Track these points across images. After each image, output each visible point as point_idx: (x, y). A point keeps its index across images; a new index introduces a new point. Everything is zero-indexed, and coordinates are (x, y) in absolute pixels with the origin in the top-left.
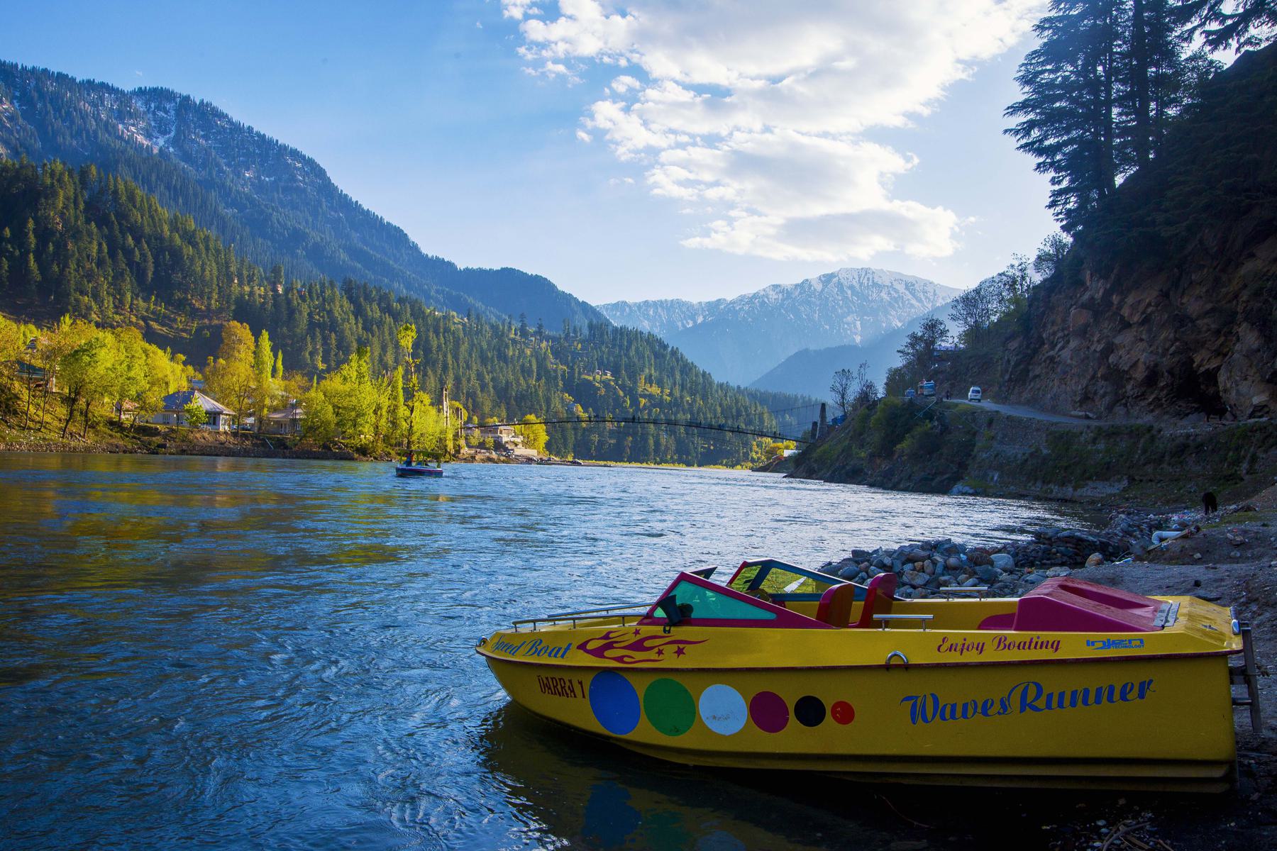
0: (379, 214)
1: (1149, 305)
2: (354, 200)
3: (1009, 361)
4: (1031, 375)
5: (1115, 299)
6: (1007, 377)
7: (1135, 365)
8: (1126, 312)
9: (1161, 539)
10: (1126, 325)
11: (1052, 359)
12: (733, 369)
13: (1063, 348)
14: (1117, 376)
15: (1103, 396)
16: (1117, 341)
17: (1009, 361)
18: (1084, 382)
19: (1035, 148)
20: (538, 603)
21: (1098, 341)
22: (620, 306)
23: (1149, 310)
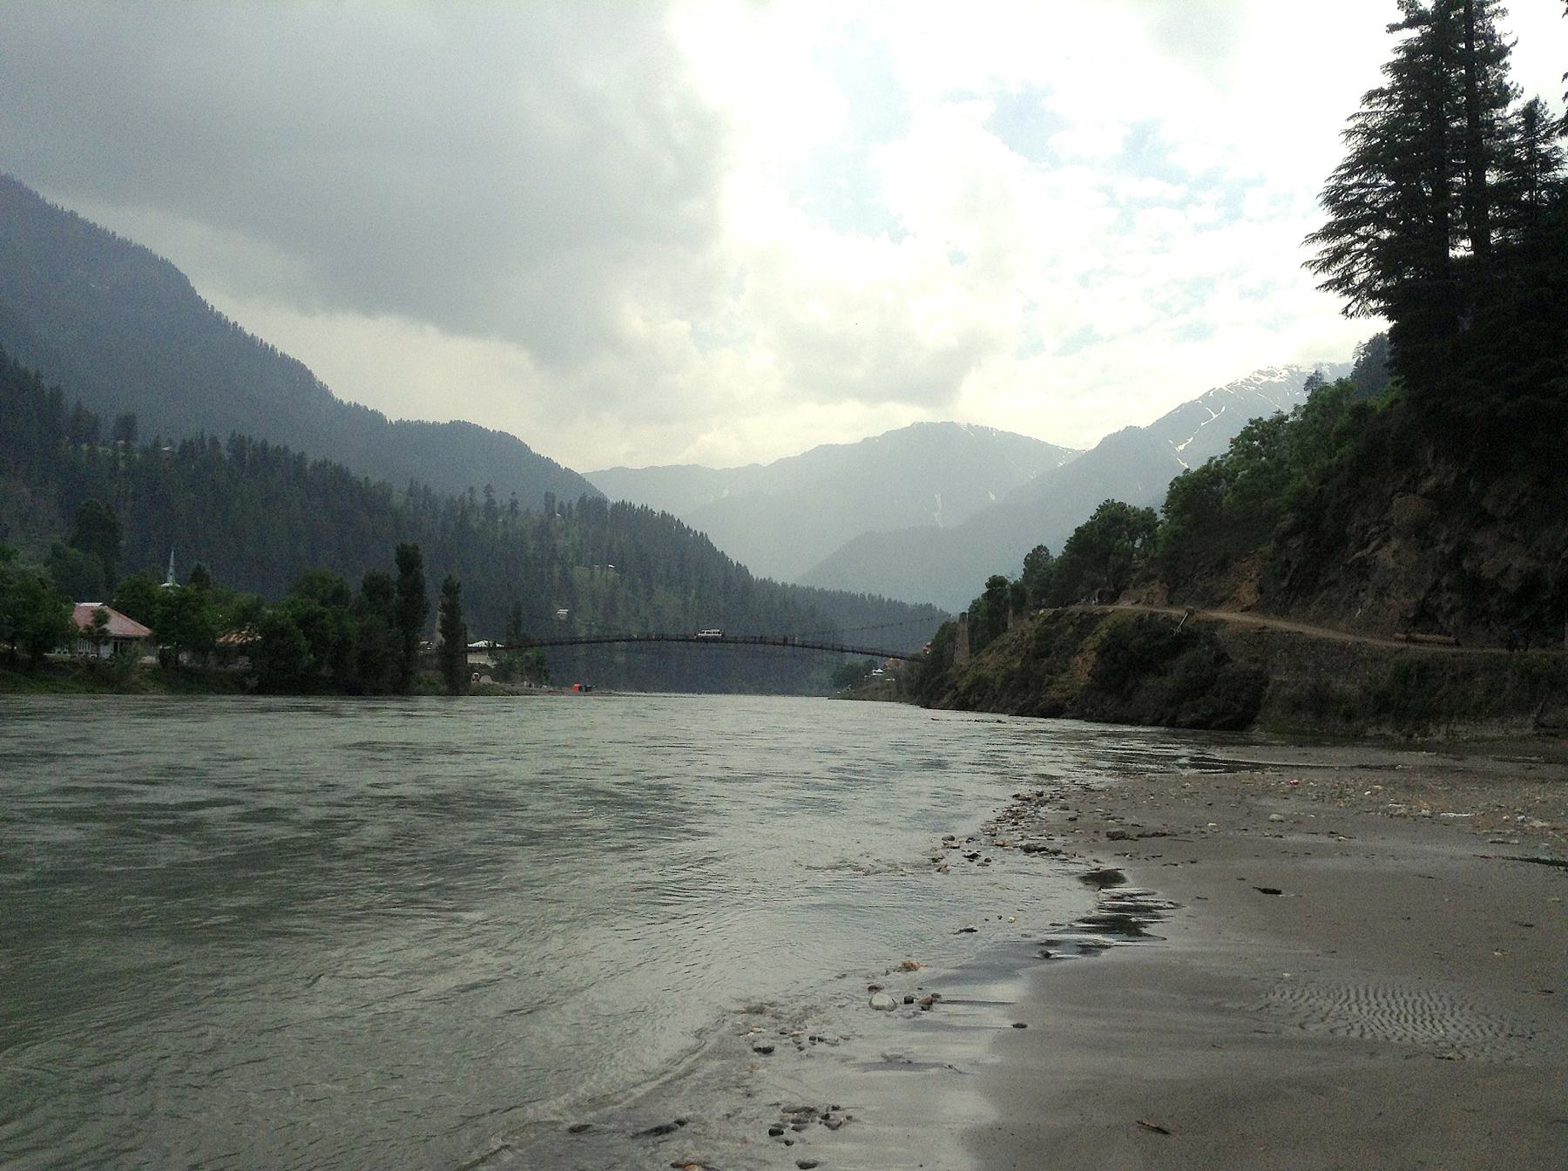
0: (269, 340)
1: (1524, 495)
2: (231, 321)
3: (1288, 563)
4: (1321, 581)
5: (1473, 486)
6: (1285, 584)
7: (1506, 570)
8: (1489, 504)
9: (1520, 727)
10: (1487, 520)
11: (1362, 562)
12: (771, 555)
13: (1379, 547)
14: (1474, 587)
15: (1452, 611)
16: (1478, 540)
17: (1288, 563)
18: (1422, 595)
19: (1342, 283)
20: (755, 1152)
21: (1447, 541)
22: (620, 473)
23: (1525, 501)
